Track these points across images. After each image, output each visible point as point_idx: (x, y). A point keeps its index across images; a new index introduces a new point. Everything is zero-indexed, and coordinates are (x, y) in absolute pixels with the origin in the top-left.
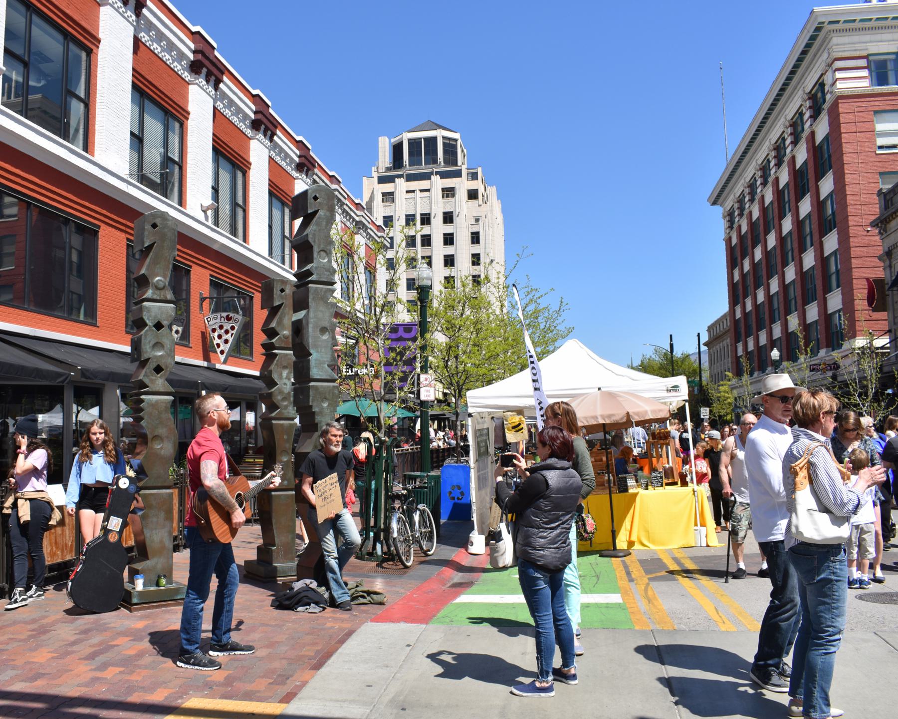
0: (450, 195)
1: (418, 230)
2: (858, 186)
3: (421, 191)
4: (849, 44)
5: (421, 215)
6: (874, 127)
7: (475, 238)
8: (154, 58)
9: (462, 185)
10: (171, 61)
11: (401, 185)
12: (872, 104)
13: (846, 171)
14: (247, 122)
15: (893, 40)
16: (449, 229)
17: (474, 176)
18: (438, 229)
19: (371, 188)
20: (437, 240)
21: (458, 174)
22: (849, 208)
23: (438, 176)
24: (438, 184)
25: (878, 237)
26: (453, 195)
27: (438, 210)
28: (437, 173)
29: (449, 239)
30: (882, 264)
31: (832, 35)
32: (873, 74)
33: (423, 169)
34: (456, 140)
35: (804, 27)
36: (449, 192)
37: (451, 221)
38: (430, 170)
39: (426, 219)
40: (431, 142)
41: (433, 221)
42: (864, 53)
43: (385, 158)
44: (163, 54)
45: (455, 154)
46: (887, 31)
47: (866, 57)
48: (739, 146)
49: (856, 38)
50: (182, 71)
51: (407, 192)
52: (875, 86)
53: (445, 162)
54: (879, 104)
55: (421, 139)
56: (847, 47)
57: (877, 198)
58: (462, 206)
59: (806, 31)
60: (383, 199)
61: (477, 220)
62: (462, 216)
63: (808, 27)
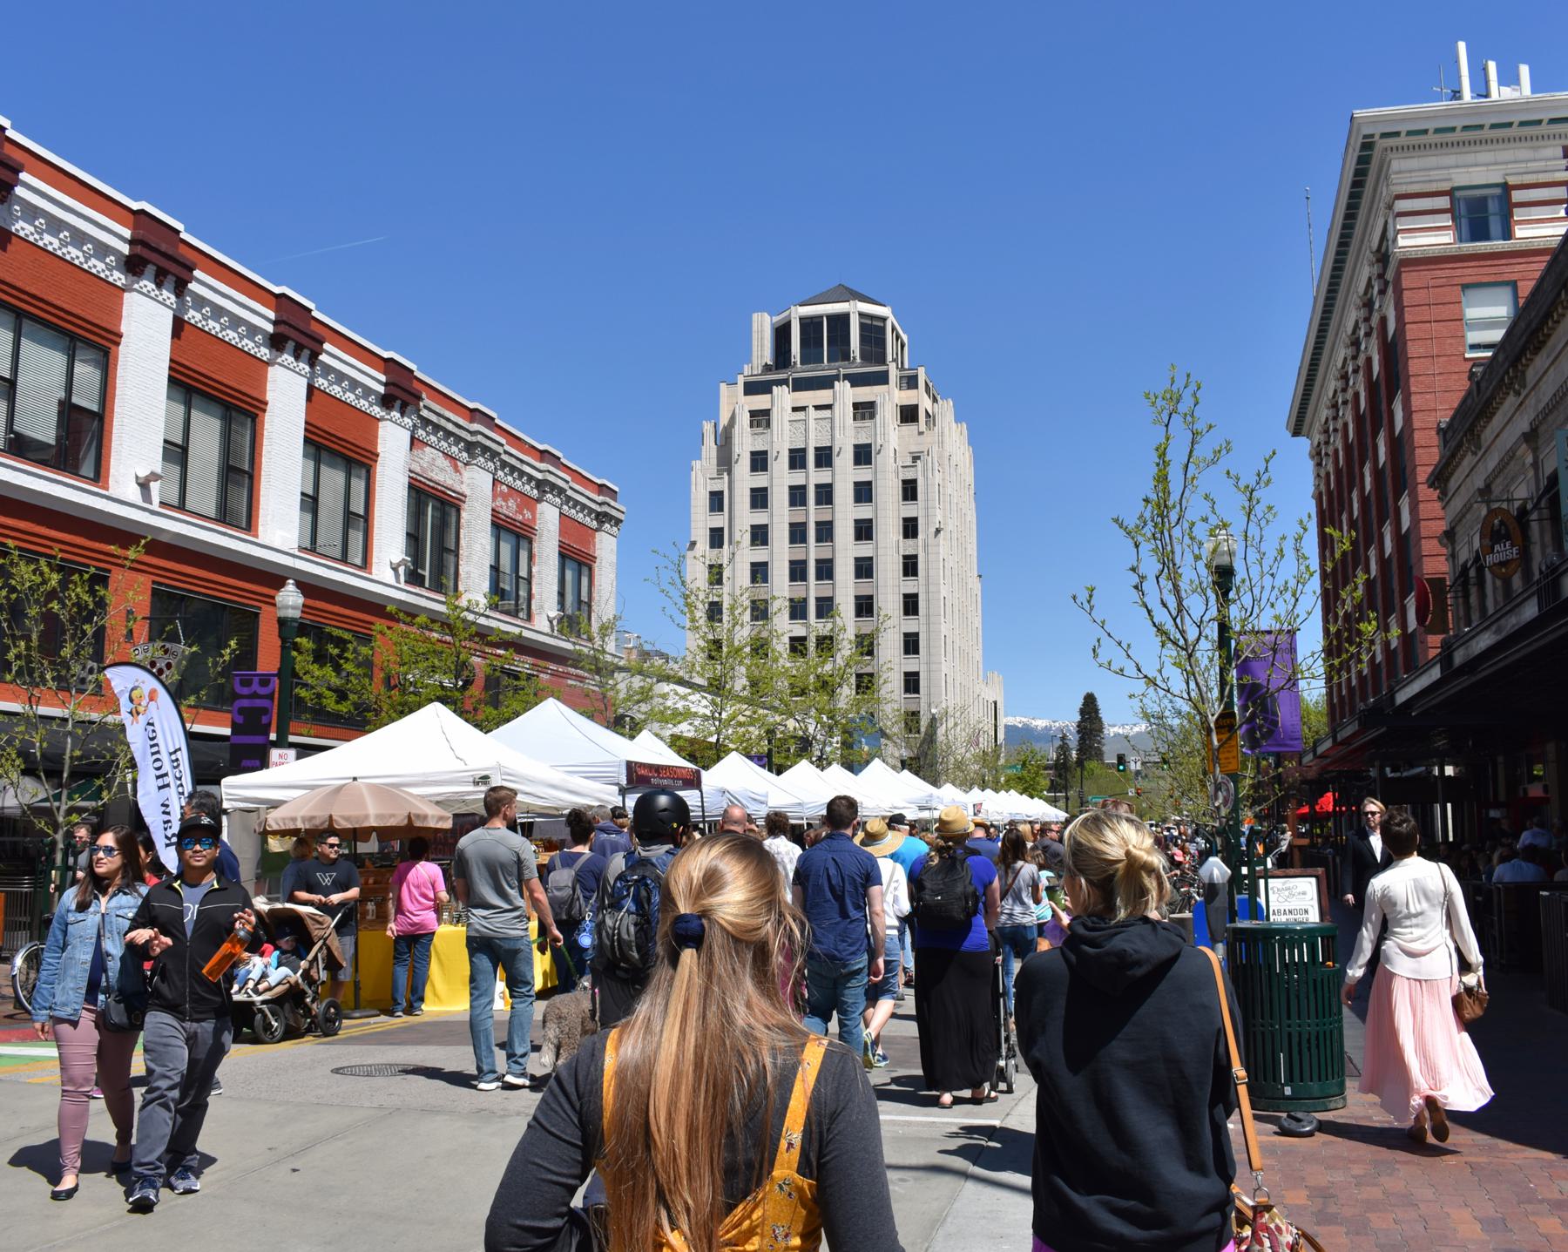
0: (867, 415)
1: (814, 476)
2: (1433, 414)
3: (817, 408)
4: (1420, 170)
5: (817, 449)
6: (1462, 312)
7: (910, 490)
8: (49, 259)
9: (890, 397)
10: (82, 260)
11: (783, 398)
12: (1458, 272)
13: (1413, 389)
14: (259, 338)
15: (1496, 164)
16: (864, 474)
17: (911, 382)
18: (845, 474)
19: (734, 402)
20: (743, 499)
21: (882, 379)
22: (1418, 451)
23: (847, 383)
24: (846, 394)
25: (1438, 505)
26: (872, 416)
27: (847, 436)
28: (846, 377)
29: (863, 492)
30: (1445, 551)
31: (1390, 155)
32: (1464, 222)
33: (825, 369)
34: (884, 319)
35: (1348, 144)
36: (864, 410)
37: (764, 468)
38: (834, 372)
39: (825, 457)
40: (841, 321)
41: (837, 461)
42: (1446, 186)
43: (763, 351)
44: (64, 250)
45: (882, 343)
46: (1484, 147)
47: (1449, 193)
48: (1307, 337)
49: (1432, 161)
50: (107, 273)
51: (795, 409)
52: (1467, 241)
53: (862, 357)
54: (1470, 273)
55: (821, 317)
56: (1416, 176)
57: (1436, 437)
58: (891, 437)
59: (1351, 150)
60: (751, 422)
61: (916, 459)
62: (888, 453)
63: (1352, 142)
